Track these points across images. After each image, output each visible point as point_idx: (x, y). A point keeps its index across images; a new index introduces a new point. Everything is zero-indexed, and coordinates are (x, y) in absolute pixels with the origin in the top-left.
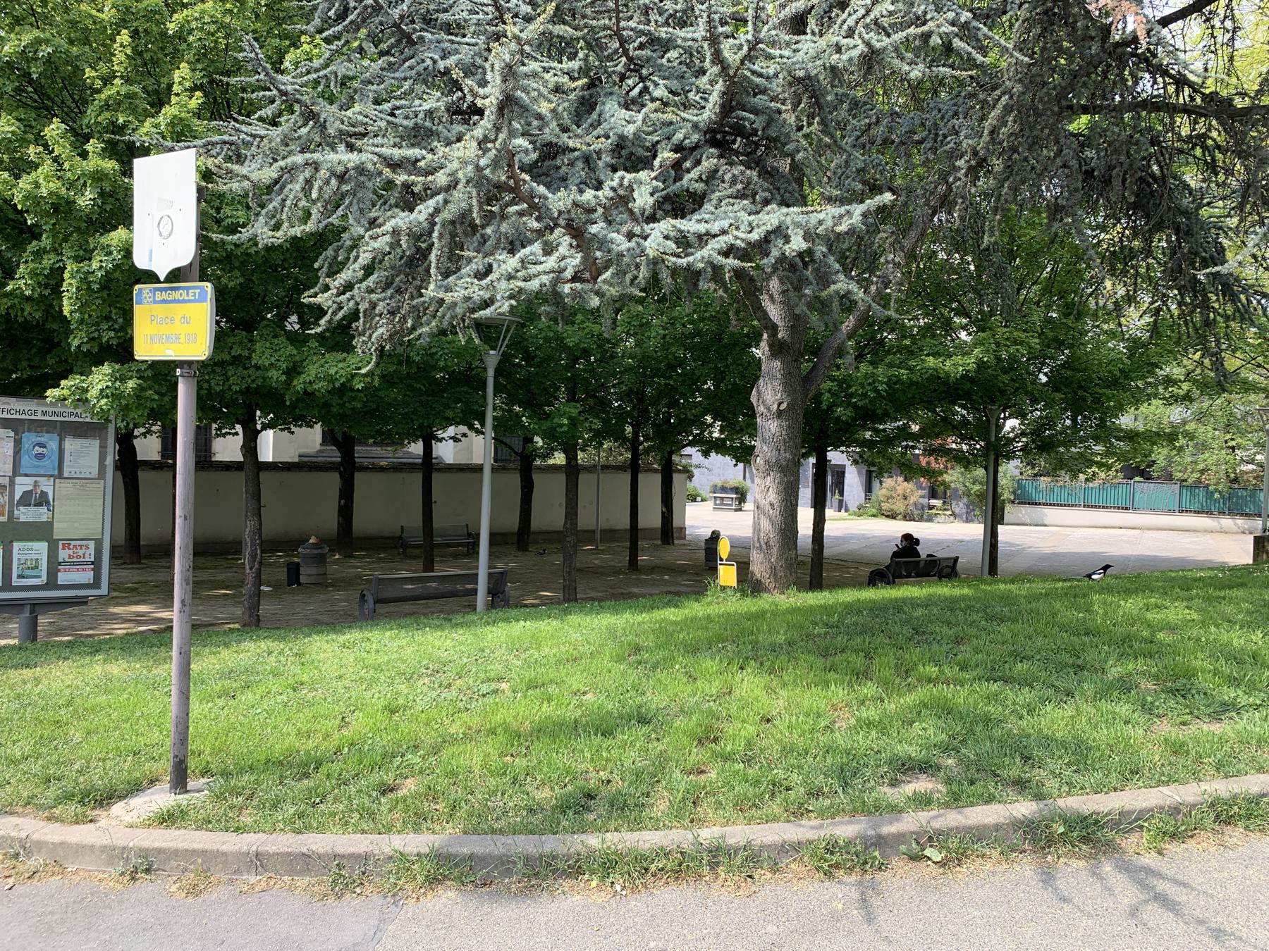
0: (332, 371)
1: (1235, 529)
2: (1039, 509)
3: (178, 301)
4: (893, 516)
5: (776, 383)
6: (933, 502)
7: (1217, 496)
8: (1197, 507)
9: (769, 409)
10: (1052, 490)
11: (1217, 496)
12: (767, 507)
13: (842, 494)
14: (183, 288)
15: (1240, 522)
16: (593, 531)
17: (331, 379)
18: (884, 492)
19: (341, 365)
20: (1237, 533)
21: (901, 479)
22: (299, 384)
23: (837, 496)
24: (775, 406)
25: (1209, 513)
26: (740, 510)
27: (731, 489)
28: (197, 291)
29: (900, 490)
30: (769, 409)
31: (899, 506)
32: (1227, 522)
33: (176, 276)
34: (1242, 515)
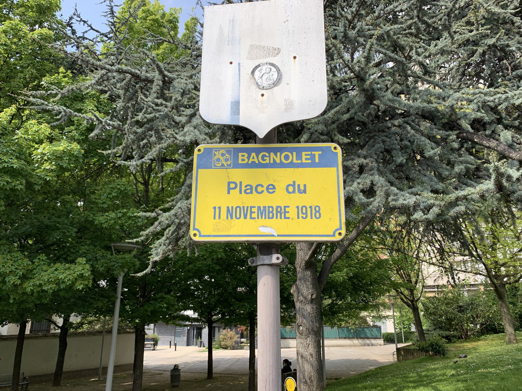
0: (61, 276)
1: (359, 344)
2: (287, 340)
3: (282, 165)
4: (226, 348)
5: (308, 283)
6: (243, 340)
7: (352, 331)
8: (343, 336)
9: (305, 298)
10: (291, 332)
11: (352, 331)
12: (309, 357)
13: (201, 338)
14: (291, 150)
15: (360, 341)
16: (98, 368)
17: (58, 282)
18: (221, 336)
19: (68, 272)
20: (359, 346)
21: (229, 330)
22: (29, 286)
23: (199, 340)
24: (310, 296)
25: (349, 338)
26: (154, 350)
27: (151, 339)
28: (317, 153)
29: (229, 335)
30: (305, 298)
31: (229, 343)
32: (356, 341)
33: (289, 132)
34: (360, 338)
